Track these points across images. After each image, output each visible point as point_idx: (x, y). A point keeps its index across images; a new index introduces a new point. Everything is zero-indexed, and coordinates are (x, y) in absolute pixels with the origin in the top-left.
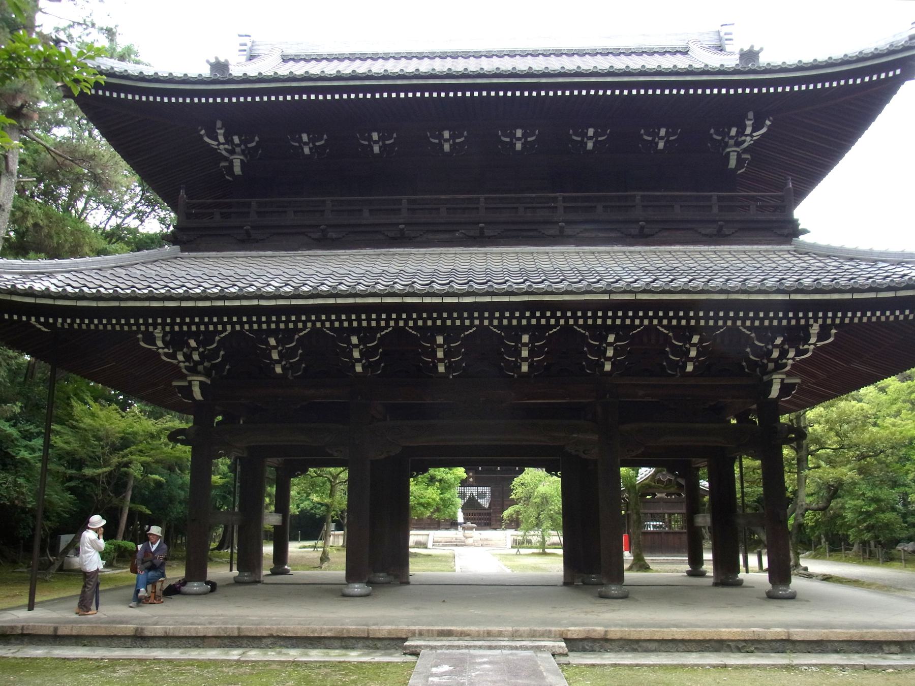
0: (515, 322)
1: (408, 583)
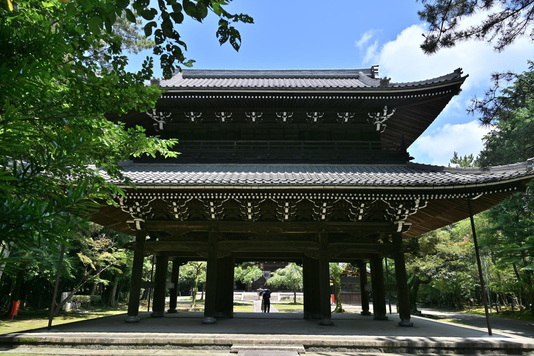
0: (282, 197)
1: (232, 317)
